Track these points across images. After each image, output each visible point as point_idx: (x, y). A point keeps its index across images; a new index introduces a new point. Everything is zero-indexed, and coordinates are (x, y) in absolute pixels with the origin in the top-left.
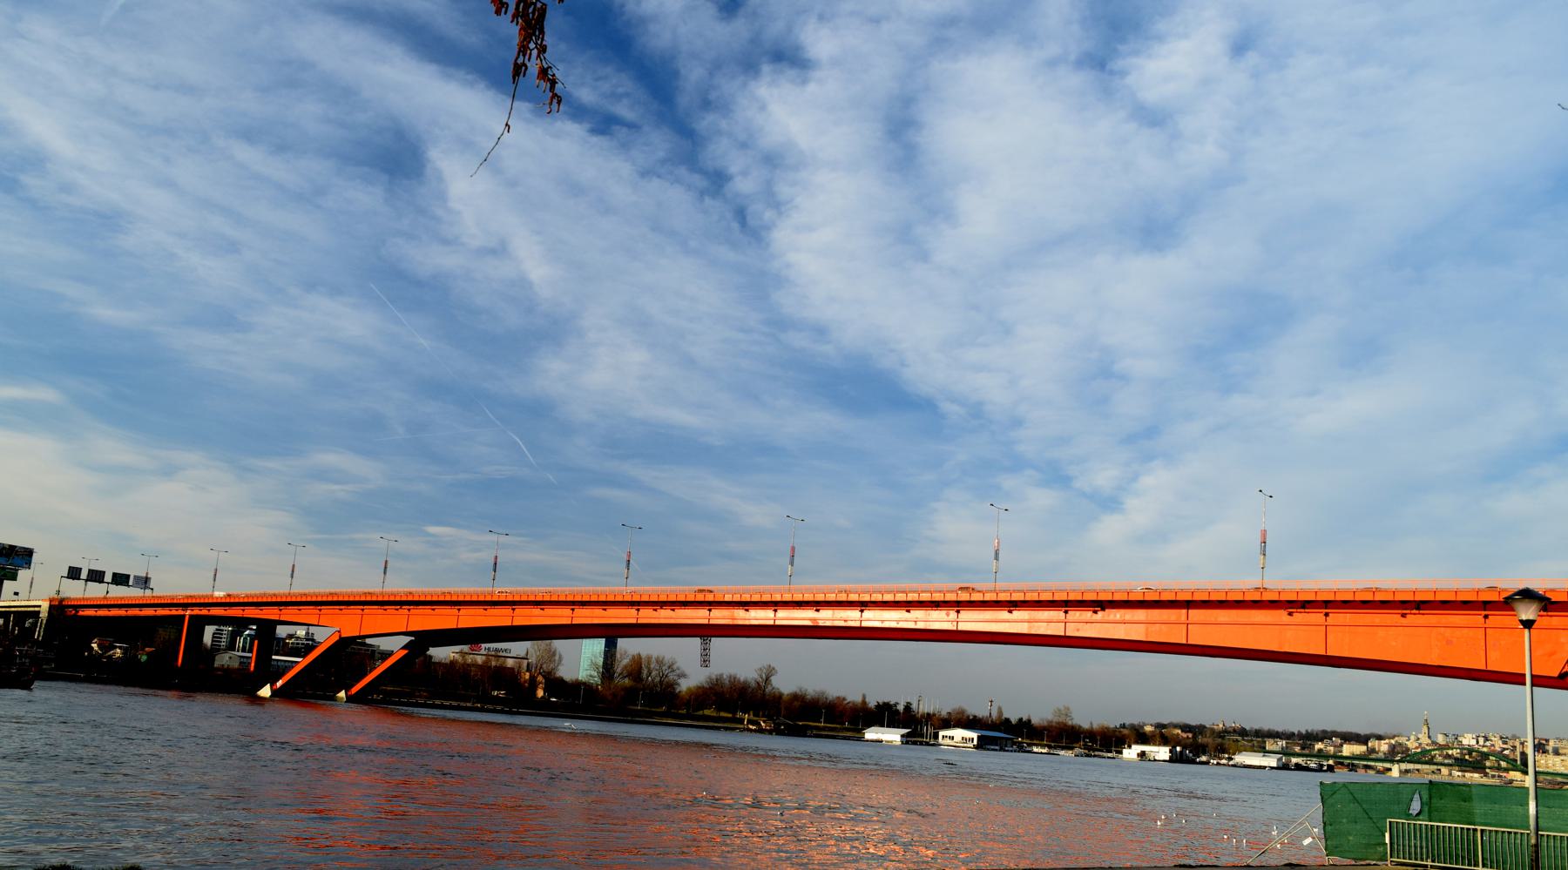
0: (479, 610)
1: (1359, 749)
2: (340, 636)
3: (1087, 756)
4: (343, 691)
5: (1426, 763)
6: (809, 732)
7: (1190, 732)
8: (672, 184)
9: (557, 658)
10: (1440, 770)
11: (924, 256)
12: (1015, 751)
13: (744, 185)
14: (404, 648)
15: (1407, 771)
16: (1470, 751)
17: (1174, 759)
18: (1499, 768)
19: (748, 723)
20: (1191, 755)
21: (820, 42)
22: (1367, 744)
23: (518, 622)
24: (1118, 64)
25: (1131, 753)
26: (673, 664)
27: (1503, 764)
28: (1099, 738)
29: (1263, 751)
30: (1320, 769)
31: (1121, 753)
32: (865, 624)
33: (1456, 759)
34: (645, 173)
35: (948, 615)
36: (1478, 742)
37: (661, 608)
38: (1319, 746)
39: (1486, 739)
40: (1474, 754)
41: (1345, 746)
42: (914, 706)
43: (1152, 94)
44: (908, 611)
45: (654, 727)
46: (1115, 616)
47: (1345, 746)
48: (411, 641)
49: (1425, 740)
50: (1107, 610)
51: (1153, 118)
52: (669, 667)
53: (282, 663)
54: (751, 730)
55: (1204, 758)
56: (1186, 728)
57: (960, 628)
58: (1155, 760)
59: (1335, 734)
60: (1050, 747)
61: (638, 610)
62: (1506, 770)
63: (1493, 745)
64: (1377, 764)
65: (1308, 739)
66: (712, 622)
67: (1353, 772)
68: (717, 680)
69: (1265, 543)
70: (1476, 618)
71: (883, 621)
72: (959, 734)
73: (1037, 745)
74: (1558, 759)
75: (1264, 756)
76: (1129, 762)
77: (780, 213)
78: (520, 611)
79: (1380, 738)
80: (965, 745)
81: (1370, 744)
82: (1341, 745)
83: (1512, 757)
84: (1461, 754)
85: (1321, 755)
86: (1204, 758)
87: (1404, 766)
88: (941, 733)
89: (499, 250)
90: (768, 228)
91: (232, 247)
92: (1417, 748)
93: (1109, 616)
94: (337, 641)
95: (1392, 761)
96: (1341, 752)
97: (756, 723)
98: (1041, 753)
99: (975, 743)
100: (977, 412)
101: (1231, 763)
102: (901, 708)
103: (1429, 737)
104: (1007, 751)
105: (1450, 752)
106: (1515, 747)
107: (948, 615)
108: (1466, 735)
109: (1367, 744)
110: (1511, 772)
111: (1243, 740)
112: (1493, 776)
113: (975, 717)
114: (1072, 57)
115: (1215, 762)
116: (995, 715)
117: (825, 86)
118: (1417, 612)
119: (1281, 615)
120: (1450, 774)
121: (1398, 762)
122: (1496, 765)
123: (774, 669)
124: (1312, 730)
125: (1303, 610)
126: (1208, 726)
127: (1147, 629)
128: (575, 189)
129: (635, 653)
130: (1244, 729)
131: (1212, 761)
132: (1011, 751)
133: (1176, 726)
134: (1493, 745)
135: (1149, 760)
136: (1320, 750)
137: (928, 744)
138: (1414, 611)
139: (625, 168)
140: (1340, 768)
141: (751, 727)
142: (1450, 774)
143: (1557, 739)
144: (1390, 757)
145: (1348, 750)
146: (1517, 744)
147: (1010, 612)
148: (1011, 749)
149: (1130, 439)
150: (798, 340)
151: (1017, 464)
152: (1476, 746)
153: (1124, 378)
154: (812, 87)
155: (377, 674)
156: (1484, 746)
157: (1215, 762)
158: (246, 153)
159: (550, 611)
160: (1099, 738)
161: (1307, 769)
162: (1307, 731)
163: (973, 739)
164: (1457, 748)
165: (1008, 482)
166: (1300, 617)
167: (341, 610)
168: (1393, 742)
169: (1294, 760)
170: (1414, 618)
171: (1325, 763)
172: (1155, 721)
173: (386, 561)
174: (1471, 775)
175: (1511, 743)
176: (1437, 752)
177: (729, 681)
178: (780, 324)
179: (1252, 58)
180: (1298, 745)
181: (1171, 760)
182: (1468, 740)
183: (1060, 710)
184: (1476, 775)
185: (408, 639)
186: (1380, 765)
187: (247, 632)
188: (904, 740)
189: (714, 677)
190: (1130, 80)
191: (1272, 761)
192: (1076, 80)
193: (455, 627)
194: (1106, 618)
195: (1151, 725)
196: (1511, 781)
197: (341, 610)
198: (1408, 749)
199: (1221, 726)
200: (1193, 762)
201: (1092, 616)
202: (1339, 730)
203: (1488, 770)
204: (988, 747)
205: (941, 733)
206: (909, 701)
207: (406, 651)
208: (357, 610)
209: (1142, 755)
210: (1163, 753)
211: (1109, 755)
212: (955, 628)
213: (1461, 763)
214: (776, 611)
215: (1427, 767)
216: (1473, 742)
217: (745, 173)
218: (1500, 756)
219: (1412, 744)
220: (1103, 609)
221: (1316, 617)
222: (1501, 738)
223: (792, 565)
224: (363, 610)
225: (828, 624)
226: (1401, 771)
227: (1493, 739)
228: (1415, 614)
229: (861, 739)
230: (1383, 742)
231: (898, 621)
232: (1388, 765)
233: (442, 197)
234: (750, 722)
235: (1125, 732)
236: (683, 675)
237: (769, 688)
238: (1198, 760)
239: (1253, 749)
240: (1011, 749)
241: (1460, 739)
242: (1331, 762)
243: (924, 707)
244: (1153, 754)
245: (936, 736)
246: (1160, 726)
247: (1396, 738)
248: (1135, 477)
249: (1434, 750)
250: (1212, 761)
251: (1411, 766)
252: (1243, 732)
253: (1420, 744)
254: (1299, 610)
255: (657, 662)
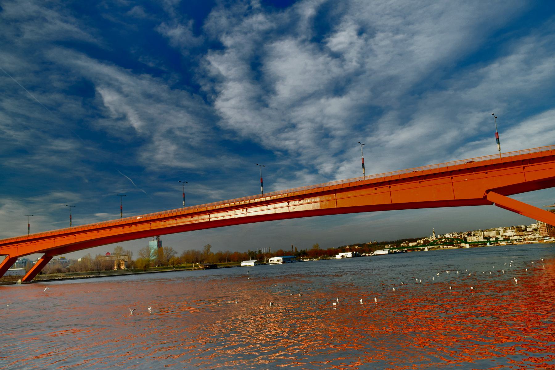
0: (61, 238)
1: (414, 244)
2: (10, 257)
3: (323, 259)
4: (20, 279)
5: (435, 245)
6: (218, 267)
7: (361, 246)
8: (182, 90)
9: (131, 253)
10: (440, 247)
11: (266, 106)
12: (297, 262)
13: (206, 88)
14: (42, 258)
15: (430, 248)
16: (448, 239)
17: (354, 255)
18: (458, 243)
19: (194, 267)
20: (359, 254)
21: (228, 41)
22: (416, 242)
23: (78, 240)
24: (324, 40)
25: (338, 257)
26: (171, 249)
27: (459, 241)
28: (309, 253)
29: (384, 249)
30: (402, 252)
31: (335, 257)
32: (211, 220)
33: (444, 242)
34: (173, 88)
35: (243, 211)
36: (450, 236)
37: (132, 226)
38: (402, 245)
39: (453, 234)
40: (450, 240)
41: (410, 243)
42: (262, 251)
43: (335, 49)
44: (227, 212)
45: (132, 276)
46: (308, 201)
47: (410, 243)
48: (44, 255)
49: (434, 238)
50: (304, 199)
51: (337, 56)
52: (170, 251)
53: (12, 271)
54: (196, 269)
55: (364, 254)
56: (359, 245)
57: (248, 216)
58: (347, 257)
59: (406, 240)
60: (310, 259)
61: (123, 228)
62: (460, 243)
63: (455, 236)
64: (420, 248)
65: (397, 244)
66: (152, 229)
67: (413, 252)
68: (187, 252)
69: (364, 163)
70: (448, 179)
71: (218, 218)
72: (276, 259)
73: (305, 259)
74: (475, 237)
75: (384, 250)
76: (339, 260)
77: (217, 97)
78: (78, 236)
79: (420, 239)
80: (278, 262)
81: (418, 242)
82: (409, 243)
83: (461, 239)
84: (446, 240)
85: (404, 247)
86: (364, 254)
87: (429, 247)
88: (270, 260)
89: (123, 117)
90: (213, 101)
91: (26, 128)
92: (432, 241)
93: (305, 201)
94: (9, 260)
95: (425, 246)
96: (409, 245)
97: (198, 266)
98: (307, 261)
99: (282, 261)
100: (286, 153)
101: (373, 254)
102: (258, 253)
103: (435, 236)
104: (294, 262)
105: (442, 240)
106: (461, 236)
107: (243, 211)
108: (446, 234)
109: (416, 242)
110: (462, 244)
111: (378, 246)
112: (456, 246)
113: (286, 252)
114: (310, 39)
115: (368, 255)
116: (294, 250)
117: (230, 55)
118: (425, 180)
119: (372, 190)
120: (443, 247)
121: (427, 246)
122: (457, 242)
123: (210, 245)
124: (399, 240)
125: (380, 187)
126: (366, 243)
127: (321, 204)
128: (148, 96)
129: (187, 250)
130: (378, 243)
131: (366, 255)
132: (296, 262)
133: (356, 245)
134: (455, 236)
135: (345, 258)
136: (402, 246)
137: (265, 264)
138: (424, 180)
139: (165, 87)
140: (409, 251)
141: (196, 268)
142: (443, 247)
143: (474, 231)
144: (425, 244)
145: (411, 244)
146: (462, 234)
147: (267, 206)
148: (295, 261)
149: (335, 155)
150: (227, 137)
151: (300, 167)
152: (450, 237)
153: (333, 137)
154: (226, 55)
155: (30, 273)
156: (452, 237)
157: (368, 255)
158: (32, 95)
159: (89, 234)
160: (309, 253)
161: (399, 253)
162: (398, 240)
163: (281, 260)
164: (444, 239)
165: (298, 173)
166: (380, 190)
167: (9, 247)
168: (424, 240)
169: (394, 250)
170: (424, 183)
171: (404, 250)
172: (349, 245)
173: (29, 225)
174: (450, 246)
175: (460, 234)
176: (438, 241)
177: (192, 252)
178: (217, 129)
179: (365, 35)
180: (395, 245)
181: (353, 257)
182: (447, 236)
183: (315, 245)
184: (451, 246)
185: (43, 254)
186: (421, 248)
187: (17, 261)
188: (255, 264)
189: (186, 252)
190: (329, 45)
191: (386, 252)
192: (311, 46)
193: (53, 247)
194: (304, 202)
195: (348, 246)
196: (462, 247)
197: (9, 247)
198: (429, 241)
199: (370, 243)
200: (361, 256)
201: (299, 202)
202: (407, 238)
203: (454, 244)
204: (287, 262)
205: (270, 260)
206: (260, 250)
207: (43, 259)
208: (14, 246)
209: (342, 256)
210: (349, 255)
211: (331, 258)
212: (246, 216)
213: (445, 243)
214: (176, 220)
215: (436, 246)
216: (449, 236)
217: (205, 85)
218: (457, 239)
219: (430, 240)
220: (303, 199)
221: (386, 188)
222: (457, 233)
223: (184, 201)
224: (17, 245)
225: (197, 222)
226: (428, 249)
227: (455, 234)
228: (424, 181)
229: (240, 266)
230: (421, 240)
231: (224, 217)
232: (424, 248)
233: (102, 103)
234: (195, 266)
235: (339, 249)
236: (176, 253)
237: (209, 253)
238: (362, 255)
239: (381, 249)
240: (295, 261)
241: (445, 236)
242: (406, 249)
243: (264, 251)
244: (346, 256)
245: (268, 261)
246: (350, 246)
247: (425, 238)
248: (338, 168)
249: (437, 240)
250: (366, 255)
251: (431, 247)
252: (377, 244)
253: (433, 239)
254: (379, 187)
255: (165, 249)
